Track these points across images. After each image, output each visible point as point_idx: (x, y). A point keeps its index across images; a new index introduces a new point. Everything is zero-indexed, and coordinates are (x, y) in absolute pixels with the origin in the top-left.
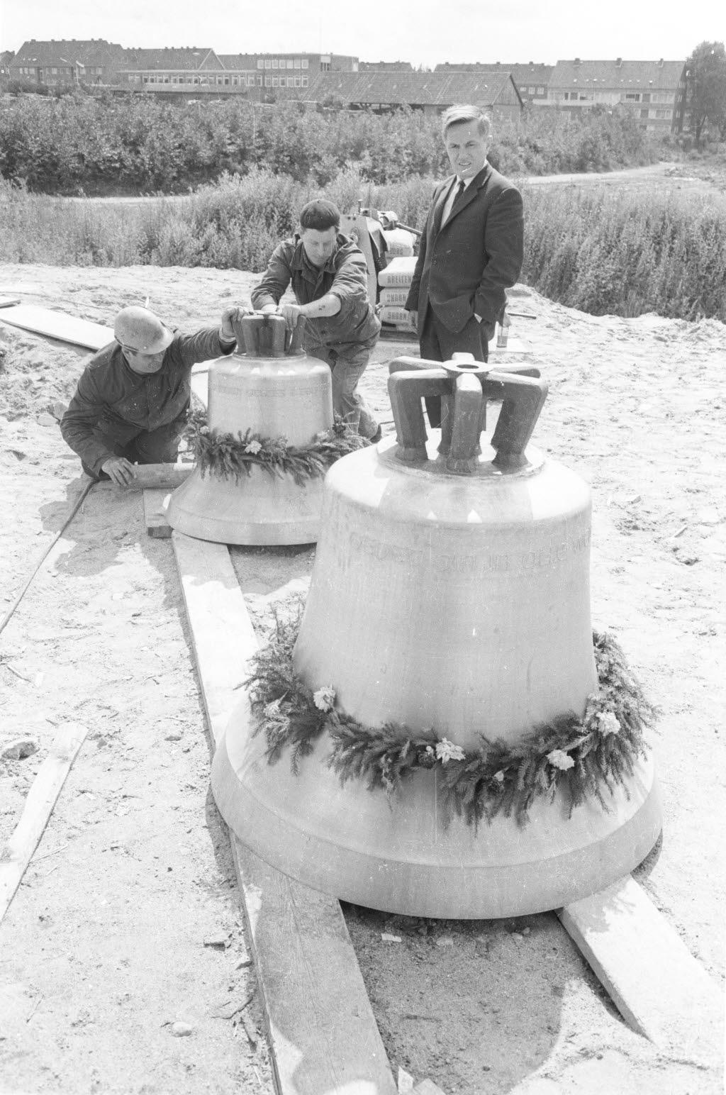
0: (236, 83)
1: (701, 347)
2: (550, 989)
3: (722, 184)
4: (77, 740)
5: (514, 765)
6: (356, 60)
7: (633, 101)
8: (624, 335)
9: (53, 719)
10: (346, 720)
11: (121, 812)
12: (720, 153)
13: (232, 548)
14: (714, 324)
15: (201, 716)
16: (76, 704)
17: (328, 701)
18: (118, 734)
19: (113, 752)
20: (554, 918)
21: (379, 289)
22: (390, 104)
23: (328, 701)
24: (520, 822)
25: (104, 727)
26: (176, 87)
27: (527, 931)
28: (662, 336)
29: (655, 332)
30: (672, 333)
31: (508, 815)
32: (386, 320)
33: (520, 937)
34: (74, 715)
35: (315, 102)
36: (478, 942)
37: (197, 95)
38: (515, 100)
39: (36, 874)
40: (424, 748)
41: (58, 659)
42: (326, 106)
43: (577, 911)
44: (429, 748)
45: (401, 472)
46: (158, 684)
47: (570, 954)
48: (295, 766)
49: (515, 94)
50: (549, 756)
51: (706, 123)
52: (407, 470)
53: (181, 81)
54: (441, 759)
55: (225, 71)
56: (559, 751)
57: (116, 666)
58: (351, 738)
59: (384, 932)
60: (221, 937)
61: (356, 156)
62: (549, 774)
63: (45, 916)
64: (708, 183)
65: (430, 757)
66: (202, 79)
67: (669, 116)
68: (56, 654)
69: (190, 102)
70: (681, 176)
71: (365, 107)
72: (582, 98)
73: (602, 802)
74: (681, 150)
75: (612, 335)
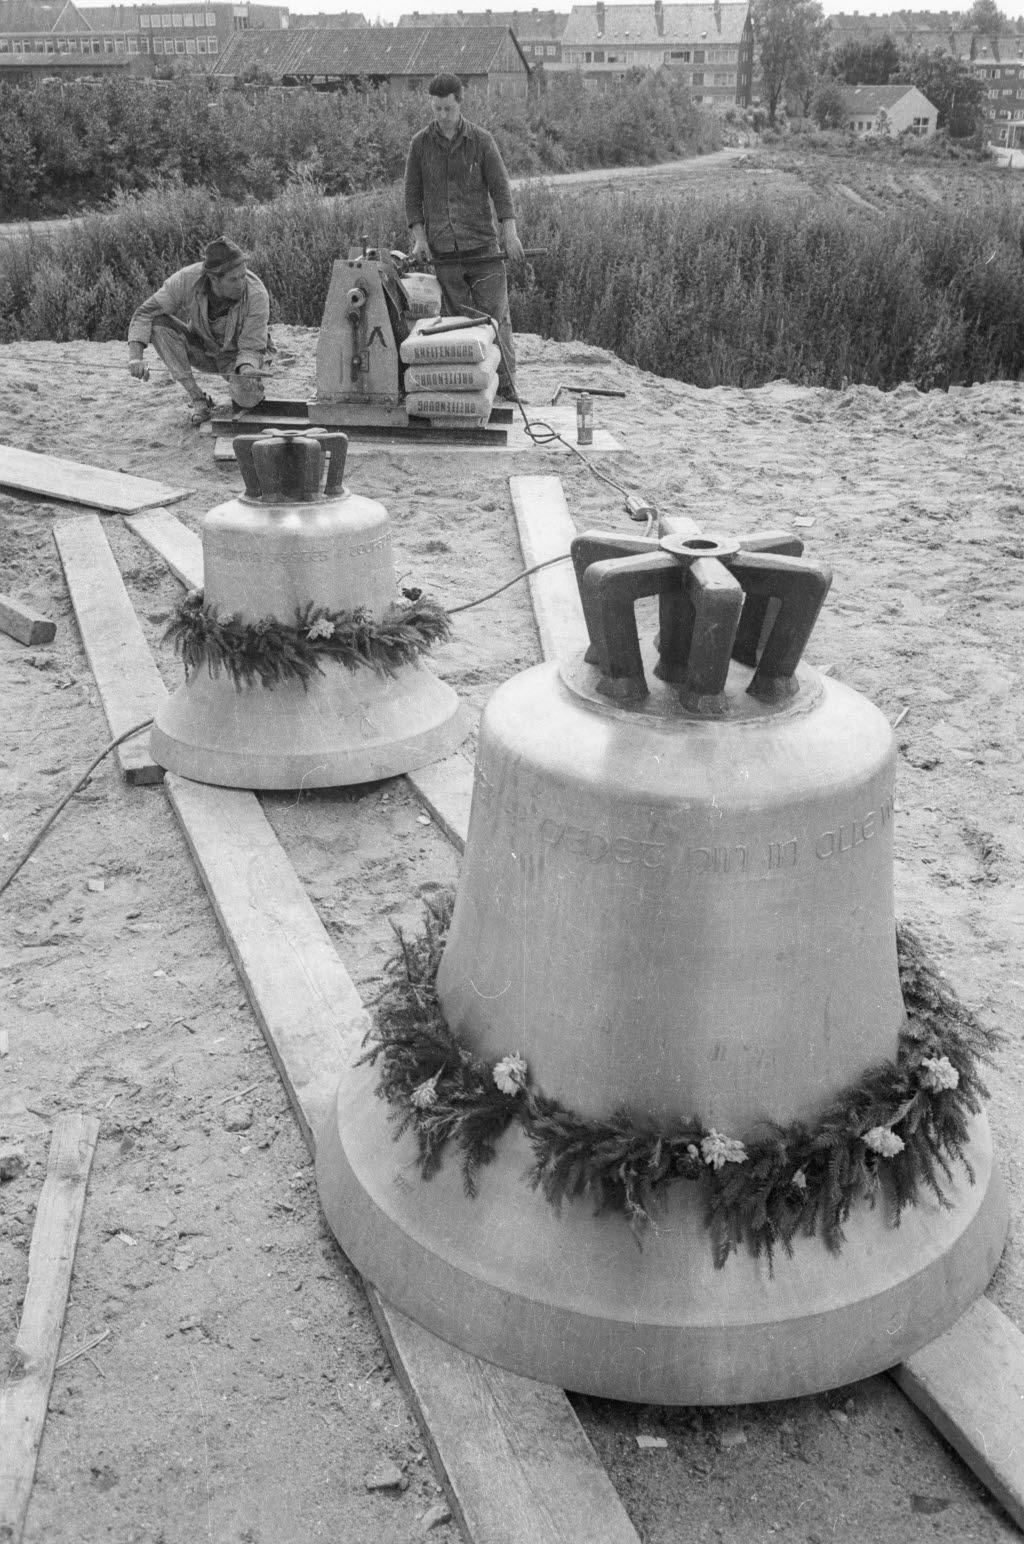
0: (111, 50)
1: (860, 428)
2: (908, 1500)
3: (812, 176)
4: (87, 1142)
5: (820, 1161)
6: (285, 11)
7: (681, 61)
8: (751, 416)
9: (39, 1108)
10: (550, 1108)
11: (182, 1263)
12: (805, 132)
13: (263, 795)
14: (869, 391)
15: (276, 1086)
16: (70, 1078)
17: (518, 1079)
18: (148, 1127)
19: (148, 1158)
20: (892, 1382)
21: (403, 367)
22: (340, 76)
23: (518, 1079)
24: (832, 1242)
25: (120, 1112)
26: (22, 58)
27: (851, 1403)
28: (802, 414)
29: (791, 408)
30: (815, 408)
31: (811, 1234)
32: (415, 413)
33: (844, 1418)
34: (69, 1096)
35: (232, 75)
36: (784, 1434)
37: (54, 69)
38: (520, 66)
39: (69, 1390)
40: (683, 1149)
41: (24, 1002)
42: (247, 81)
43: (927, 1365)
44: (692, 1148)
45: (613, 718)
46: (192, 1032)
47: (922, 1436)
48: (470, 1183)
49: (517, 55)
50: (866, 1138)
51: (783, 90)
52: (623, 715)
53: (28, 49)
54: (712, 1162)
55: (92, 32)
56: (881, 1129)
57: (120, 1007)
58: (563, 1137)
59: (638, 1432)
60: (391, 1474)
61: (300, 154)
62: (869, 1164)
63: (101, 1468)
64: (792, 177)
65: (695, 1163)
66: (60, 44)
67: (732, 82)
68: (21, 994)
69: (45, 80)
70: (756, 167)
71: (306, 80)
72: (612, 60)
73: (939, 1193)
74: (751, 129)
75: (735, 418)
